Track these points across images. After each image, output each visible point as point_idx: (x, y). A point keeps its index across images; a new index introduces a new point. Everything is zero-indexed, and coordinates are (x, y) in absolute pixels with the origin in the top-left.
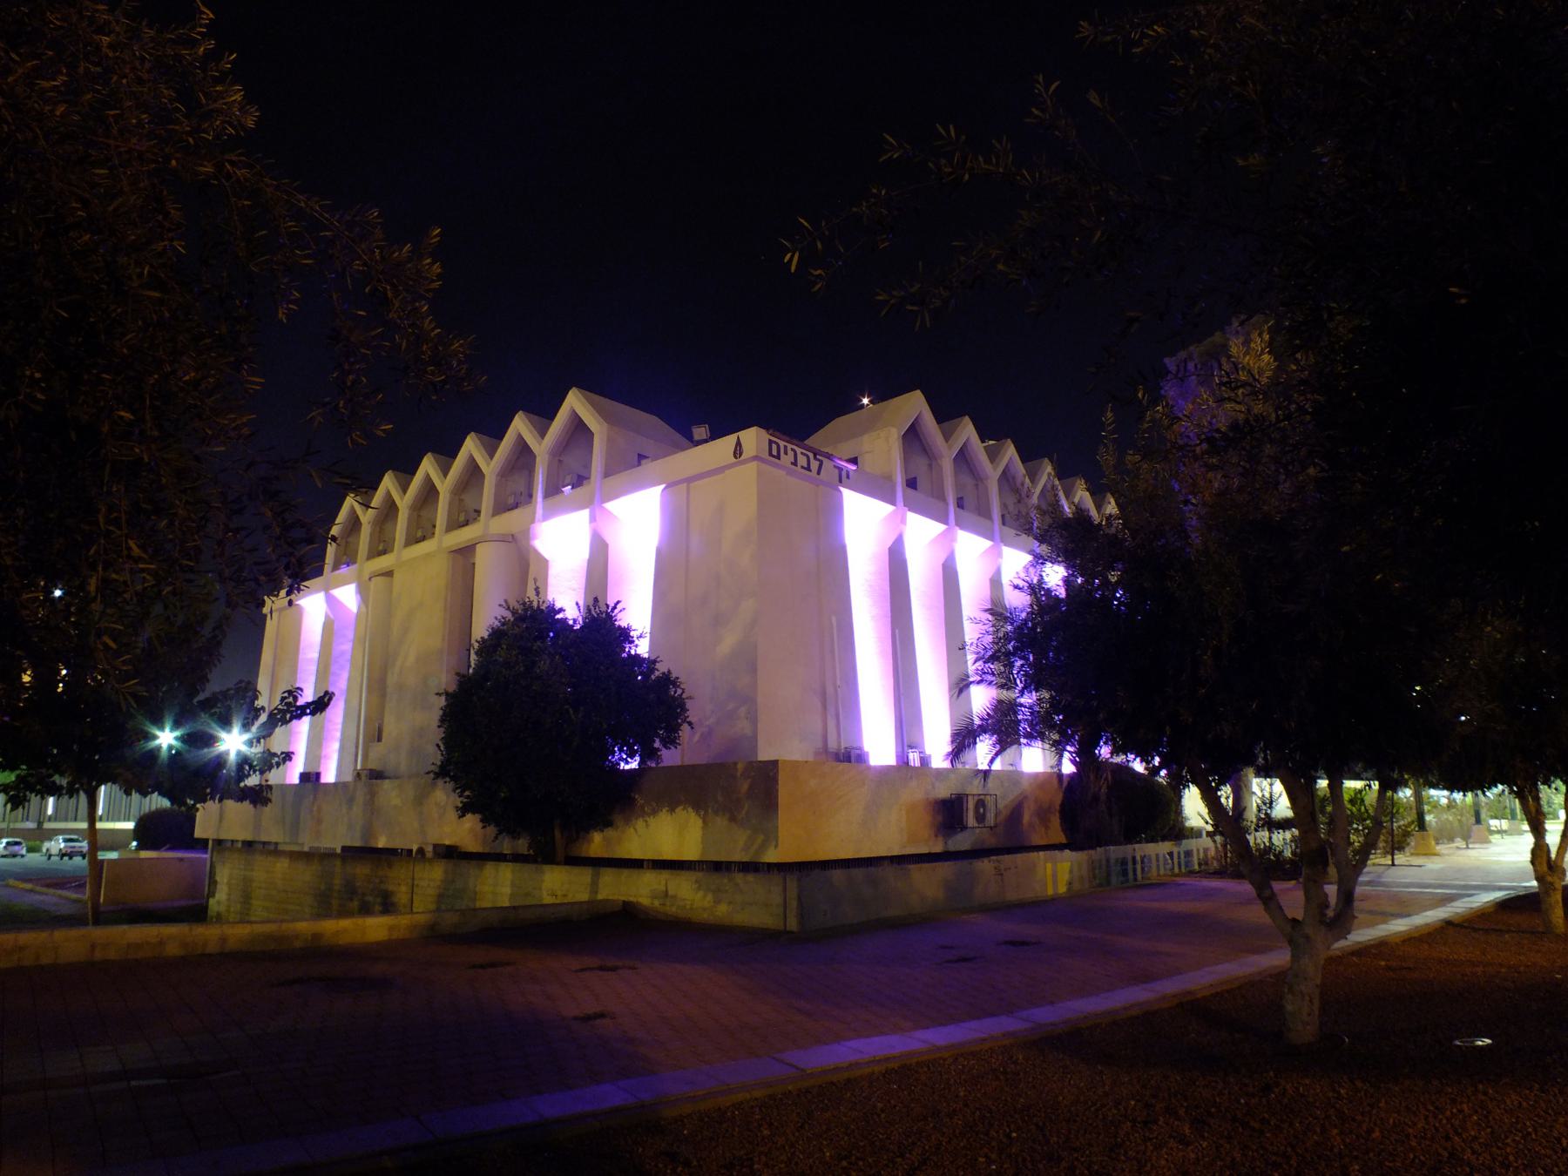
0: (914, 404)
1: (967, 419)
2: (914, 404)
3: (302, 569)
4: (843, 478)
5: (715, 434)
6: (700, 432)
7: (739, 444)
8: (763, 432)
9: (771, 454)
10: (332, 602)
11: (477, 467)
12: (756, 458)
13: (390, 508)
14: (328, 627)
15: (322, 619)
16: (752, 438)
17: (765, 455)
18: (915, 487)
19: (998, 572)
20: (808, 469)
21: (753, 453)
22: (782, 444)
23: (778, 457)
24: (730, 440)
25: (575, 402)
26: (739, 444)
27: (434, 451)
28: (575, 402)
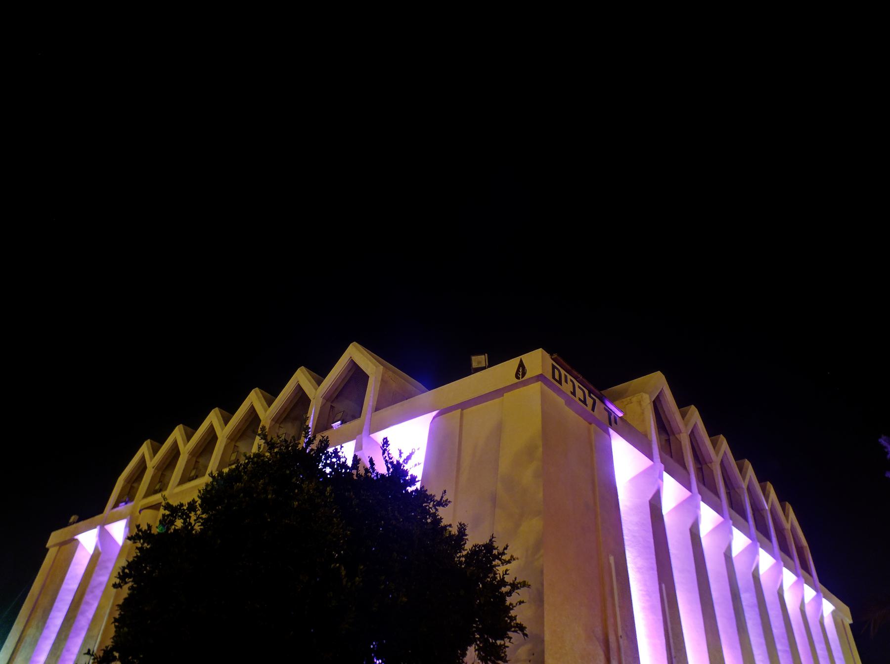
0: (657, 381)
1: (693, 406)
2: (657, 381)
3: (91, 509)
4: (612, 422)
5: (493, 362)
6: (478, 360)
7: (521, 365)
8: (547, 355)
9: (554, 377)
10: (104, 536)
11: (257, 416)
12: (540, 378)
13: (175, 453)
14: (95, 558)
15: (91, 551)
16: (537, 360)
17: (549, 376)
18: (669, 452)
19: (729, 549)
20: (584, 402)
21: (539, 372)
22: (563, 372)
23: (560, 382)
24: (514, 363)
25: (355, 353)
26: (521, 365)
27: (220, 407)
28: (355, 353)
